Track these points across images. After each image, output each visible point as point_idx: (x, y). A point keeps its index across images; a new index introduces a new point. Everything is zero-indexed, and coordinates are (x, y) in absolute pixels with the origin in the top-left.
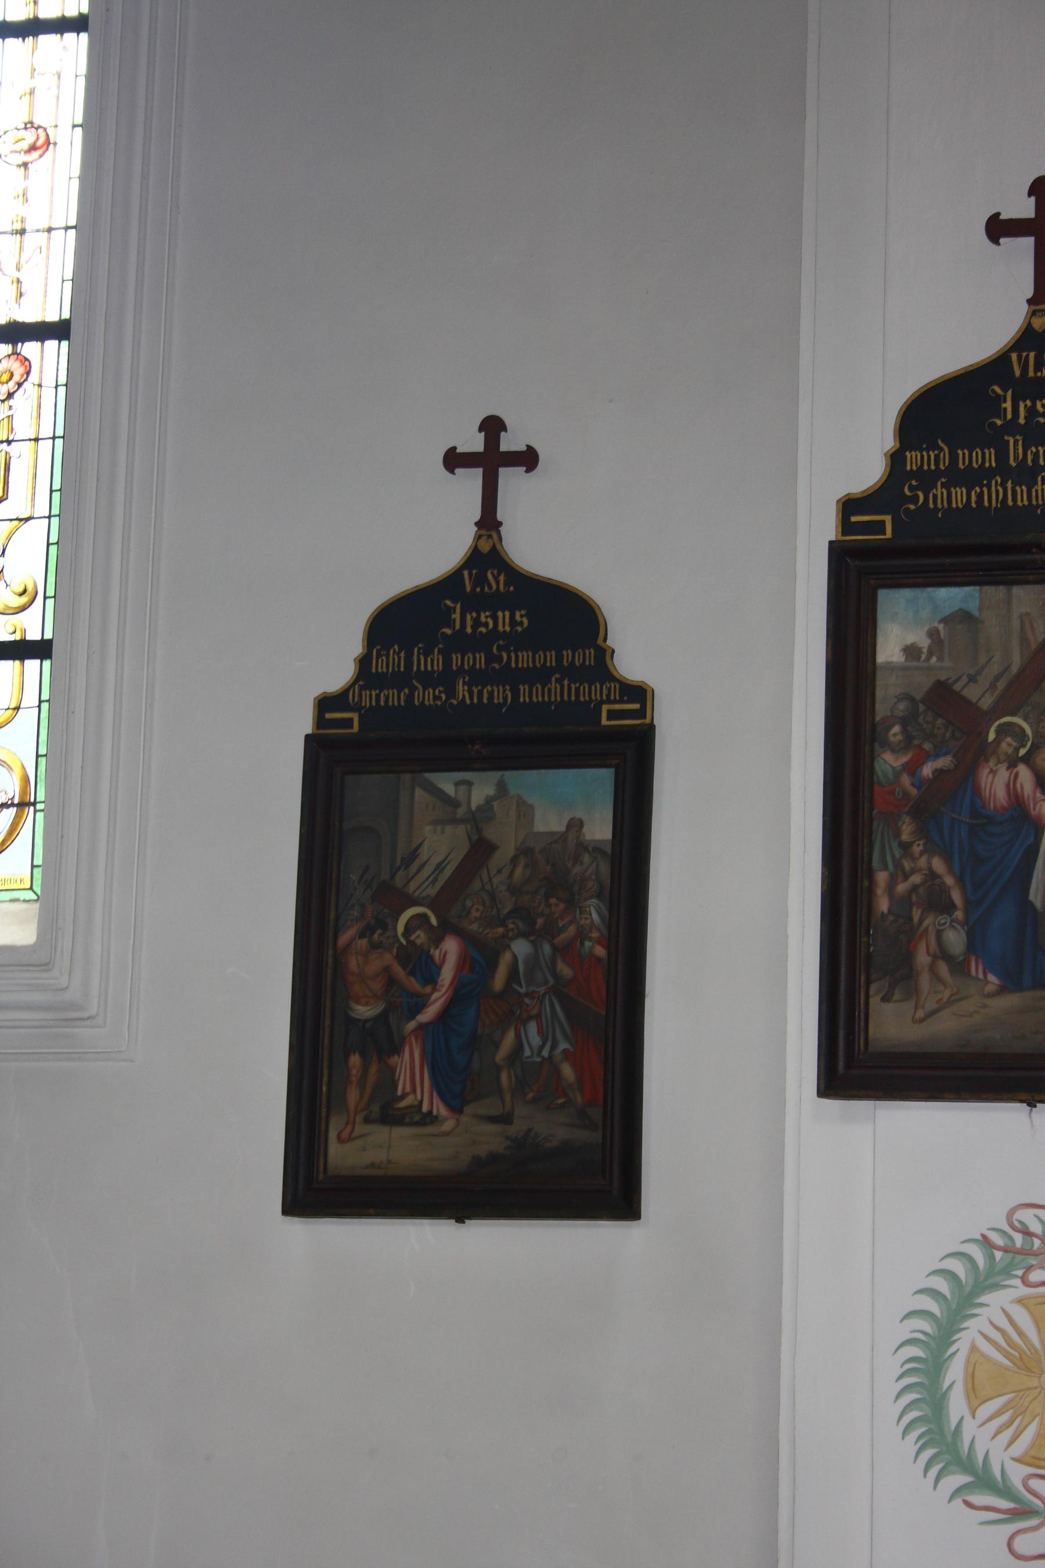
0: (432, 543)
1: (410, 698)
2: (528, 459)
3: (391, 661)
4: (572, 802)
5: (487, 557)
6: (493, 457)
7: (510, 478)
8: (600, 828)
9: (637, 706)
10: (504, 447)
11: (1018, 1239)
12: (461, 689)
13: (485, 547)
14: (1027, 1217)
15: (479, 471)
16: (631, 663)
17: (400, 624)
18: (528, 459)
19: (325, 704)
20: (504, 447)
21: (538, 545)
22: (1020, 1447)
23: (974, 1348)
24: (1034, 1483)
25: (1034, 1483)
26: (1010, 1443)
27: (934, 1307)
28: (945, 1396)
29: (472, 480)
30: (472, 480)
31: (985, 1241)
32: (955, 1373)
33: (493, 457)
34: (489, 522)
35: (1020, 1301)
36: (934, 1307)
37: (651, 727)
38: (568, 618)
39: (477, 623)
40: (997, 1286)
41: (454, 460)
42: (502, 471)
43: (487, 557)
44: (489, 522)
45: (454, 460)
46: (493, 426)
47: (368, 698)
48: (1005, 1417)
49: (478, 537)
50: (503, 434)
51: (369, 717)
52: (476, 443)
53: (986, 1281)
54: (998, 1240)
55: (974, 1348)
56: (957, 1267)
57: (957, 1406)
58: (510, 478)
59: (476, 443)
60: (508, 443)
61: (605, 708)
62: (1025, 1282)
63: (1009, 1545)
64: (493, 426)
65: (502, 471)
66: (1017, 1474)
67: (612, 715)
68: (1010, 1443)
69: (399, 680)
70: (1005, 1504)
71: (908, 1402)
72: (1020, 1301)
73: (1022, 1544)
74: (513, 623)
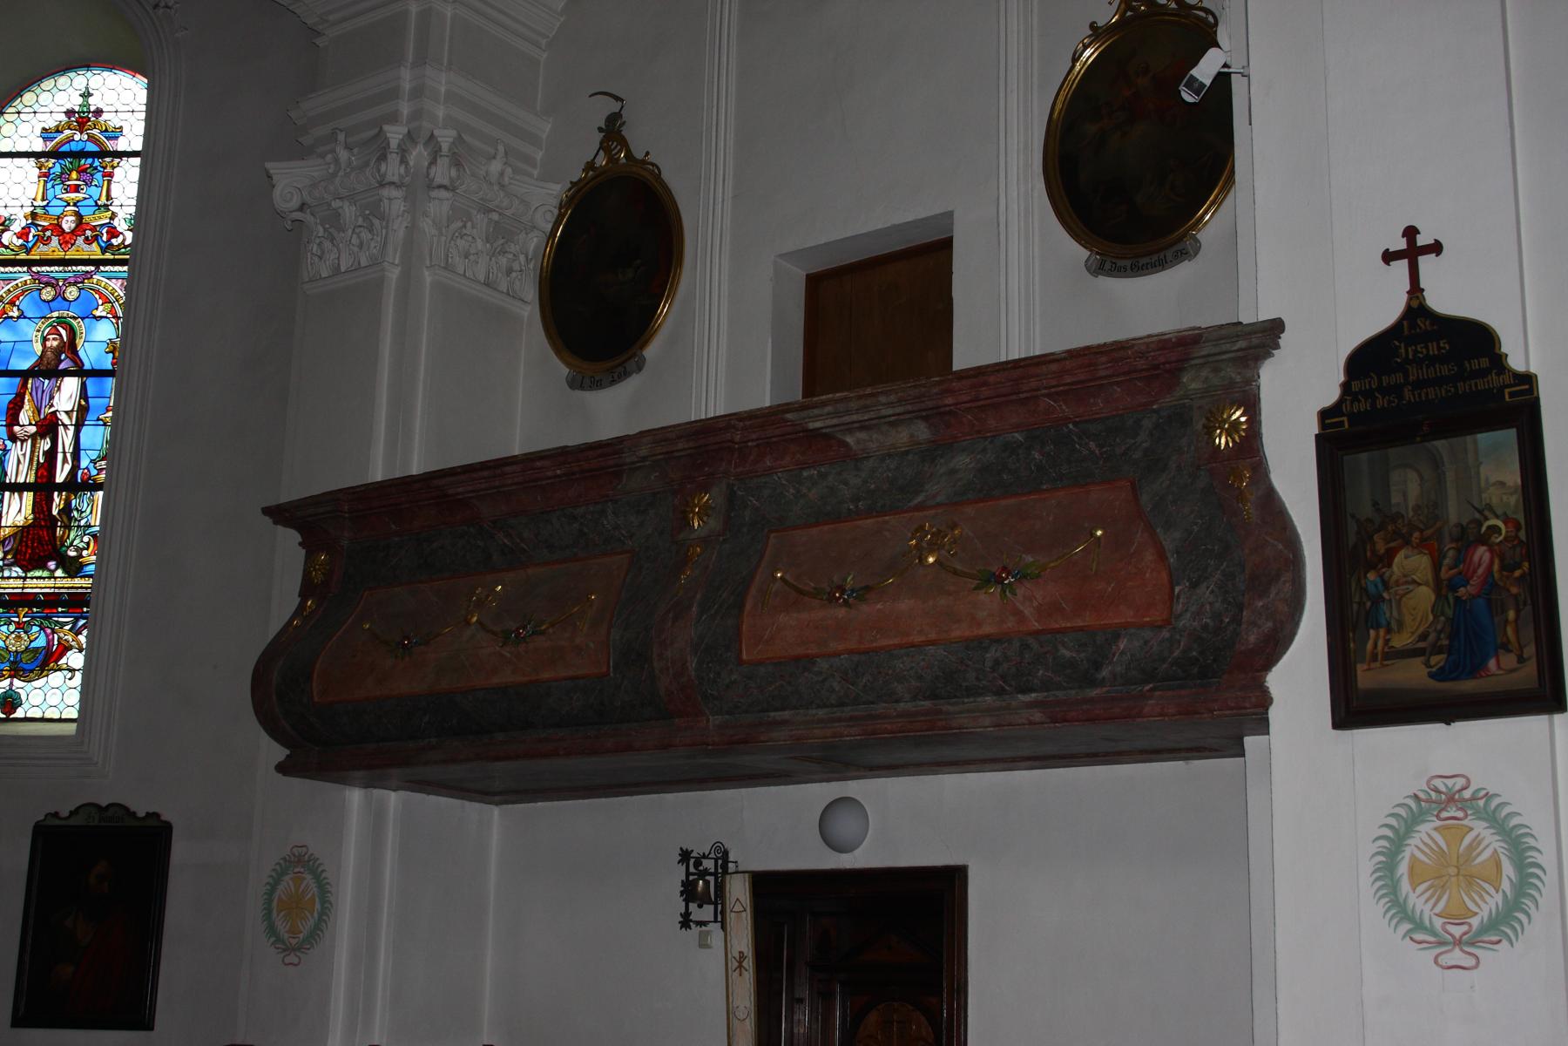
0: (1378, 307)
1: (1373, 405)
2: (1436, 248)
3: (1355, 386)
4: (1493, 458)
5: (1417, 310)
6: (1413, 250)
7: (1425, 262)
8: (1512, 475)
9: (1485, 362)
10: (1419, 243)
11: (1433, 794)
12: (1407, 393)
13: (1415, 304)
14: (1438, 783)
15: (1405, 261)
16: (1405, 297)
17: (1367, 362)
18: (1436, 248)
19: (1324, 415)
20: (1419, 243)
21: (1444, 299)
22: (1438, 909)
23: (1413, 855)
24: (1450, 928)
25: (1450, 928)
26: (1435, 905)
27: (1389, 833)
28: (1399, 880)
29: (1402, 266)
30: (1402, 266)
31: (1416, 796)
32: (1403, 869)
33: (1413, 250)
34: (1415, 289)
35: (1435, 829)
36: (1389, 833)
37: (1538, 399)
38: (1475, 340)
39: (1416, 352)
40: (1424, 821)
41: (1388, 257)
42: (1421, 259)
43: (1417, 310)
44: (1415, 289)
45: (1388, 257)
46: (1411, 233)
47: (1363, 406)
48: (1427, 895)
49: (1410, 299)
50: (280, 753)
51: (1353, 418)
52: (1402, 244)
53: (284, 873)
54: (1422, 795)
55: (1413, 855)
56: (1393, 821)
57: (1405, 886)
58: (1425, 262)
59: (1402, 244)
60: (1422, 240)
61: (1507, 391)
62: (1437, 816)
63: (1436, 962)
64: (1411, 233)
65: (1421, 259)
66: (1438, 923)
67: (1512, 395)
68: (1435, 905)
69: (1368, 394)
70: (1432, 939)
71: (844, 856)
72: (1435, 829)
73: (1444, 960)
74: (1439, 348)
